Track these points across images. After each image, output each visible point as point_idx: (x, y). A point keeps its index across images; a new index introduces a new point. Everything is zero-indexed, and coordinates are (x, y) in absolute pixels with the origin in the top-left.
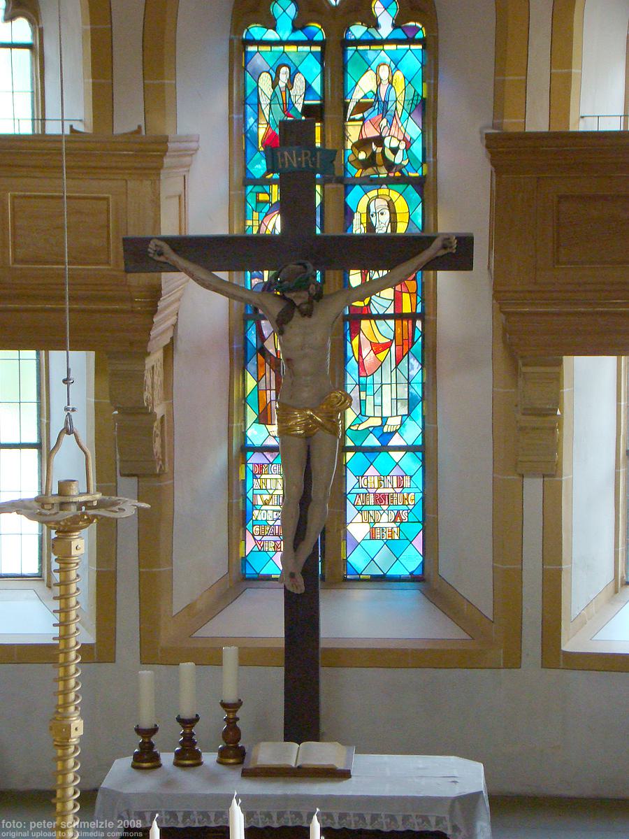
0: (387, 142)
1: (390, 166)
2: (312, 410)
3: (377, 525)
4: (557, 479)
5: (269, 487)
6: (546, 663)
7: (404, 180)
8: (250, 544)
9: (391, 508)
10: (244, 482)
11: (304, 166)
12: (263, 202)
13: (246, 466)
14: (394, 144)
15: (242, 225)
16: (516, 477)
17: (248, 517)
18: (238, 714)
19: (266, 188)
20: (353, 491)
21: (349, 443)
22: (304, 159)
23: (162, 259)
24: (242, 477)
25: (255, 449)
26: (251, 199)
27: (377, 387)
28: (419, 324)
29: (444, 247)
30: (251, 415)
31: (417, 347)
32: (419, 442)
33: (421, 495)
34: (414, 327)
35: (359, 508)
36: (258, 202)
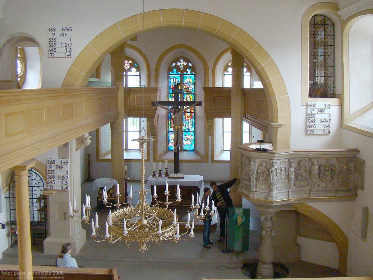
26: (170, 96)
30: (170, 127)
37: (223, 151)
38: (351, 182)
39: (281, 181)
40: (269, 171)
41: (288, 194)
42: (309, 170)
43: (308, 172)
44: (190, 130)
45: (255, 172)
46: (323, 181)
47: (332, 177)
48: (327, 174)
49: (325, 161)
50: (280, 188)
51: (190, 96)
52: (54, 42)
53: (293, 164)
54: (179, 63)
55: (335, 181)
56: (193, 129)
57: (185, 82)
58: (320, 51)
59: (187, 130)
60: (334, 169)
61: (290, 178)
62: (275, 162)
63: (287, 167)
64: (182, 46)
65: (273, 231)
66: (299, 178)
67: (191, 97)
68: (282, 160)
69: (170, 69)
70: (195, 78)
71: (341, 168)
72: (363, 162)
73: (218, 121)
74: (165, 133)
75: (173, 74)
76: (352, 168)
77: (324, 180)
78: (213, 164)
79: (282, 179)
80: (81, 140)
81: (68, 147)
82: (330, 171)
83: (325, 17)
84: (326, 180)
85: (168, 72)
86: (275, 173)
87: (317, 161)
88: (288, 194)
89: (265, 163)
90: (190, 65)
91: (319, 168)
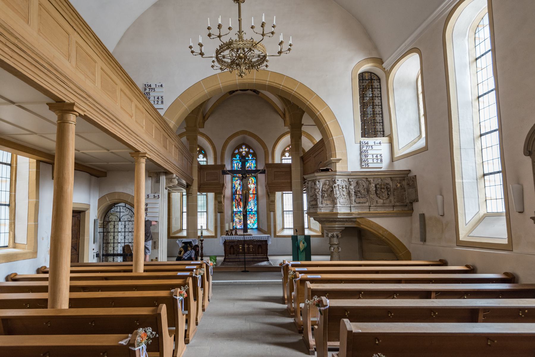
26: (234, 179)
30: (234, 207)
31: (256, 198)
37: (283, 228)
38: (406, 198)
39: (343, 197)
40: (332, 188)
41: (351, 209)
42: (367, 189)
43: (366, 190)
44: (253, 210)
45: (321, 190)
46: (380, 198)
47: (388, 194)
48: (383, 191)
49: (380, 180)
50: (343, 203)
51: (252, 178)
52: (148, 96)
53: (352, 182)
54: (241, 150)
55: (392, 198)
56: (255, 209)
57: (247, 166)
58: (369, 110)
59: (250, 210)
60: (389, 186)
61: (350, 195)
62: (337, 179)
63: (347, 185)
64: (244, 132)
65: (340, 248)
66: (358, 196)
67: (253, 180)
68: (342, 179)
69: (233, 155)
70: (256, 163)
71: (395, 187)
72: (414, 177)
73: (278, 194)
74: (230, 212)
75: (236, 159)
76: (406, 187)
77: (381, 197)
78: (275, 238)
79: (344, 195)
80: (170, 180)
81: (160, 183)
82: (386, 189)
83: (372, 74)
84: (383, 197)
85: (232, 157)
86: (337, 188)
87: (373, 180)
88: (351, 209)
89: (328, 182)
90: (251, 151)
91: (376, 186)
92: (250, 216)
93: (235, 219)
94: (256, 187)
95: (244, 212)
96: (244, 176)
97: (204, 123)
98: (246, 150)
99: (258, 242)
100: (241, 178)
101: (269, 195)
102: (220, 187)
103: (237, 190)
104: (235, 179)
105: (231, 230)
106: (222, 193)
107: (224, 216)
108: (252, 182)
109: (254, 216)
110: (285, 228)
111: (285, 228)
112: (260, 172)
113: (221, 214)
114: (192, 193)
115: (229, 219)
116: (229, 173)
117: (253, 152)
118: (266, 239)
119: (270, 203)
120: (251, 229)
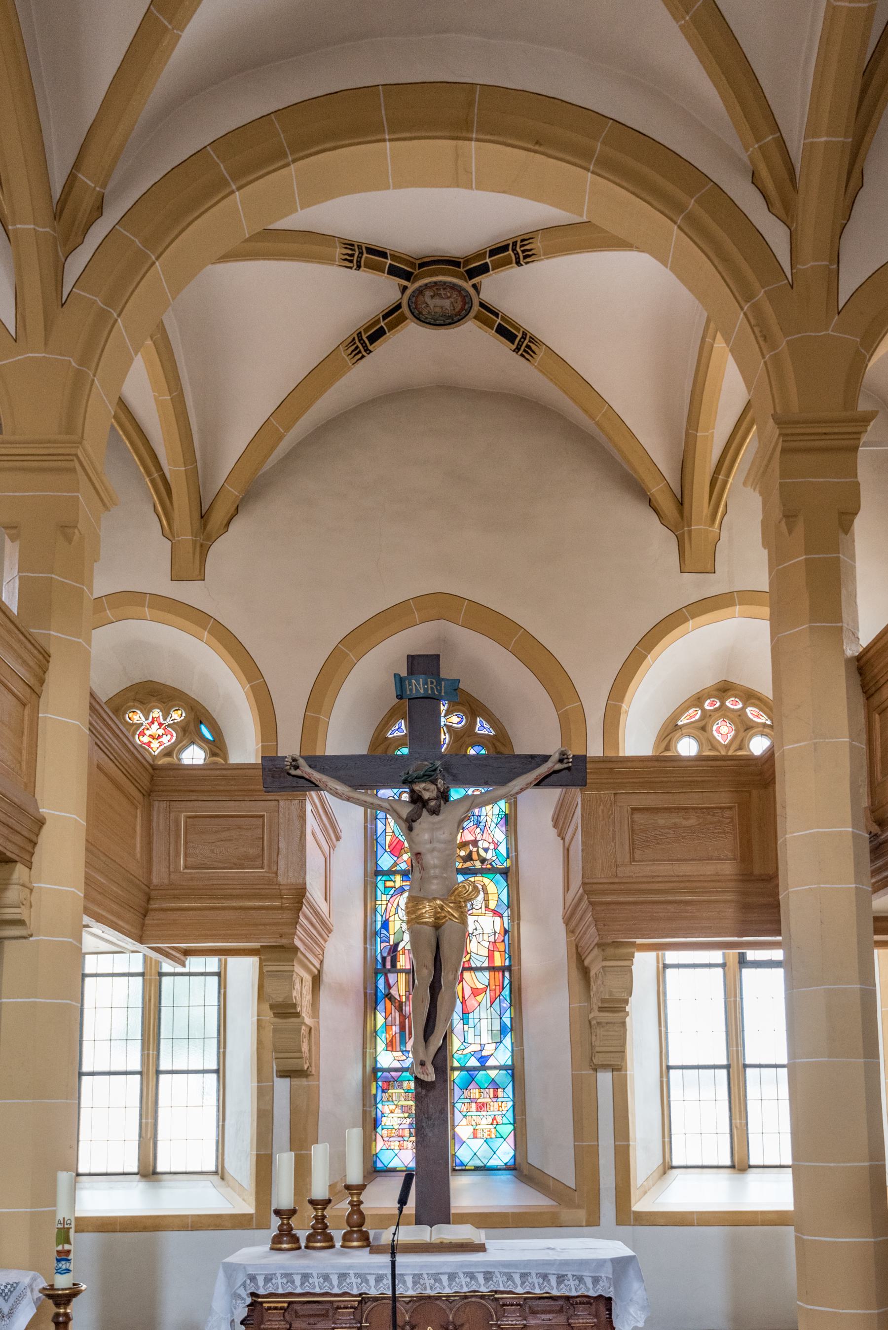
0: (480, 844)
1: (483, 861)
2: (441, 900)
3: (478, 1127)
4: (623, 1073)
5: (394, 1099)
6: (620, 1222)
7: (493, 870)
8: (380, 1144)
9: (489, 1113)
10: (375, 1096)
11: (430, 692)
12: (389, 887)
13: (377, 1083)
14: (486, 845)
15: (373, 903)
16: (591, 1072)
17: (378, 1124)
18: (362, 1198)
19: (392, 877)
20: (459, 1101)
21: (456, 1064)
22: (430, 686)
23: (298, 772)
24: (374, 1092)
25: (383, 1070)
26: (380, 885)
27: (476, 1021)
28: (507, 974)
29: (561, 761)
30: (381, 1045)
31: (506, 992)
32: (509, 1063)
33: (511, 1103)
34: (503, 976)
35: (464, 1114)
36: (385, 887)
37: (667, 1167)
44: (491, 1062)
59: (473, 1062)
67: (492, 888)
74: (355, 1075)
92: (475, 1093)
93: (386, 1110)
94: (506, 932)
95: (423, 1064)
96: (428, 791)
97: (203, 551)
98: (454, 719)
99: (533, 1312)
100: (405, 812)
101: (585, 972)
102: (281, 908)
103: (396, 945)
104: (389, 884)
105: (348, 1187)
106: (296, 949)
107: (313, 1096)
108: (486, 900)
109: (496, 1096)
110: (673, 1167)
111: (675, 1163)
112: (544, 769)
113: (297, 1081)
114: (20, 923)
115: (352, 1107)
116: (316, 776)
117: (493, 733)
118: (604, 1289)
119: (595, 1013)
120: (477, 1169)
